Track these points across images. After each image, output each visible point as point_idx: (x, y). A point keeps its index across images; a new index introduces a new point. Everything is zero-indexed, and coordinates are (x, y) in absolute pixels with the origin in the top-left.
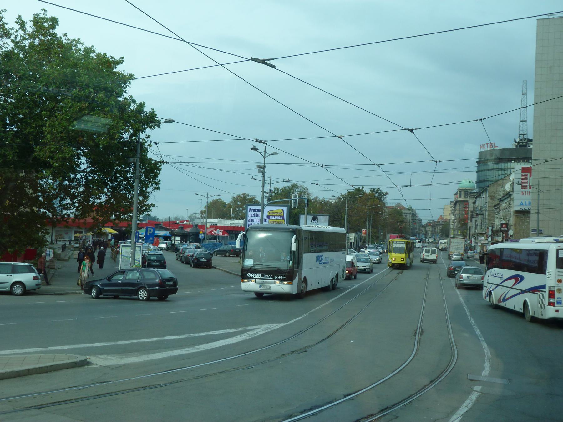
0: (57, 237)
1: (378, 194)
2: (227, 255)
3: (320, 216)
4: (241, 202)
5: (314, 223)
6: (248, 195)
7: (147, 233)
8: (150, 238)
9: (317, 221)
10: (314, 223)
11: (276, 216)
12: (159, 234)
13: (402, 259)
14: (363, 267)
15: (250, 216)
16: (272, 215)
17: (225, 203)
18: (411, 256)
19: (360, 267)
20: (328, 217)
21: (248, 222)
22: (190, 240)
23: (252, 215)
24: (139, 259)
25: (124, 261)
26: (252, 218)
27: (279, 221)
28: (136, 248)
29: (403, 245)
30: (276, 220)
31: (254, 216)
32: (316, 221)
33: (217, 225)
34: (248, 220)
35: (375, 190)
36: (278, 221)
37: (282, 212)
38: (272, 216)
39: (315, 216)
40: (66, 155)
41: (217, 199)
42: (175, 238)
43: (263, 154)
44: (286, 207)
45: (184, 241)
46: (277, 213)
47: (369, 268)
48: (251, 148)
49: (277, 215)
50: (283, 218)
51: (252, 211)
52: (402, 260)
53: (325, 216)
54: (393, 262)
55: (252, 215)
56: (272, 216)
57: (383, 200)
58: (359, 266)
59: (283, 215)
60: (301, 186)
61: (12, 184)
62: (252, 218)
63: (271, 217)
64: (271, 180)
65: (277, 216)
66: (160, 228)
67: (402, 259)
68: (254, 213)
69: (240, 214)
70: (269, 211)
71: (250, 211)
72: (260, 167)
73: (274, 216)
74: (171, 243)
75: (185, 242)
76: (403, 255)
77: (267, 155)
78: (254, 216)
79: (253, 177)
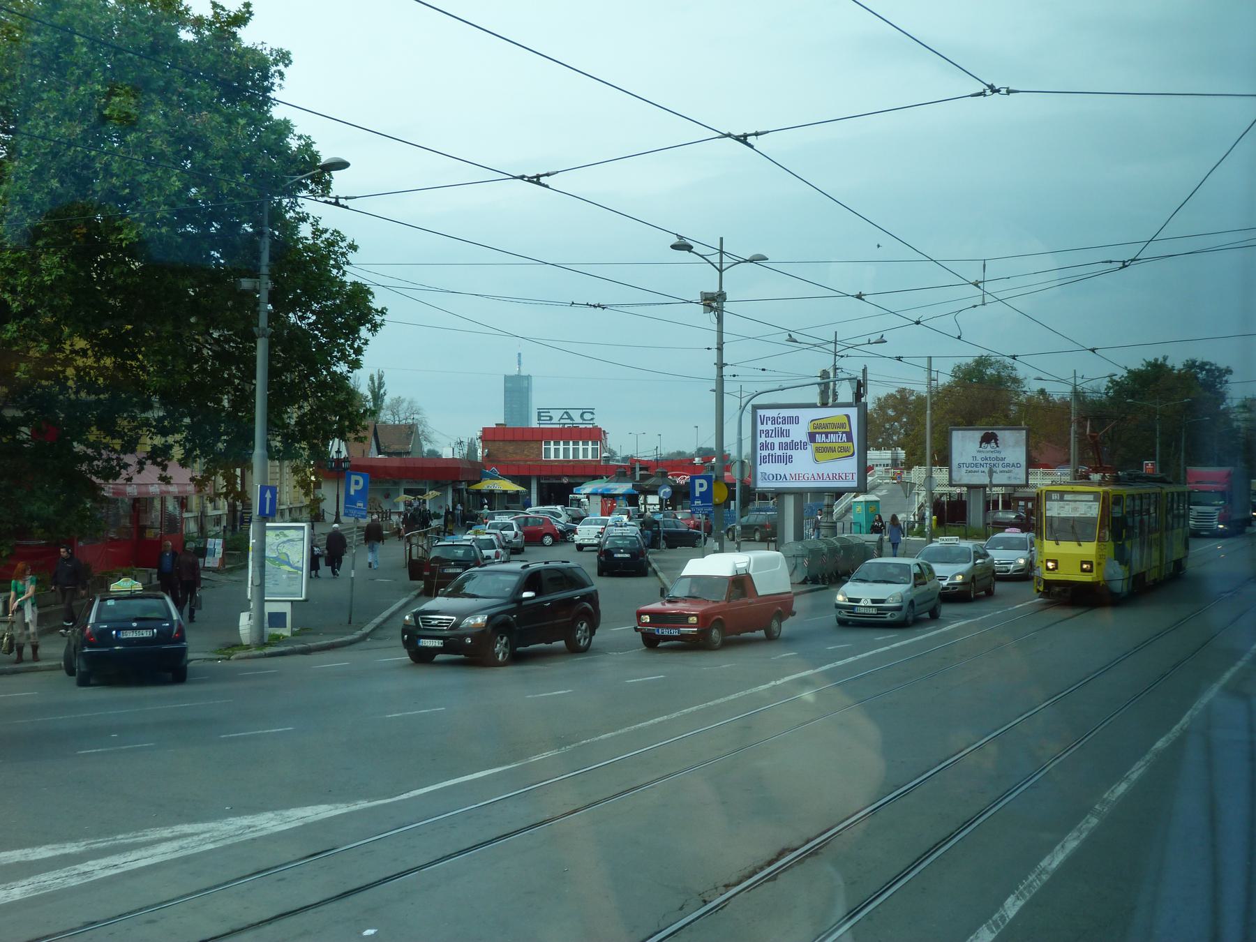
1: (1204, 372)
2: (757, 537)
3: (1002, 432)
4: (895, 408)
6: (912, 392)
7: (349, 491)
8: (358, 504)
9: (997, 444)
11: (831, 433)
12: (616, 489)
13: (1085, 566)
14: (874, 601)
15: (763, 435)
16: (821, 430)
20: (1025, 431)
21: (759, 452)
23: (767, 434)
26: (769, 440)
28: (269, 533)
29: (1090, 507)
30: (831, 445)
31: (773, 435)
32: (993, 444)
34: (759, 446)
35: (1197, 364)
37: (847, 422)
39: (990, 432)
40: (46, 278)
42: (645, 500)
43: (716, 259)
46: (834, 426)
47: (899, 609)
48: (672, 244)
49: (836, 430)
50: (850, 439)
51: (769, 422)
52: (1083, 570)
53: (1016, 431)
54: (1049, 576)
55: (768, 433)
56: (822, 433)
57: (1221, 387)
58: (858, 600)
59: (847, 429)
62: (769, 440)
63: (817, 435)
65: (834, 433)
66: (619, 476)
67: (1085, 566)
68: (773, 427)
69: (895, 438)
70: (812, 421)
71: (762, 424)
72: (709, 296)
73: (827, 434)
74: (639, 511)
75: (670, 508)
76: (1089, 549)
78: (773, 435)
79: (790, 335)
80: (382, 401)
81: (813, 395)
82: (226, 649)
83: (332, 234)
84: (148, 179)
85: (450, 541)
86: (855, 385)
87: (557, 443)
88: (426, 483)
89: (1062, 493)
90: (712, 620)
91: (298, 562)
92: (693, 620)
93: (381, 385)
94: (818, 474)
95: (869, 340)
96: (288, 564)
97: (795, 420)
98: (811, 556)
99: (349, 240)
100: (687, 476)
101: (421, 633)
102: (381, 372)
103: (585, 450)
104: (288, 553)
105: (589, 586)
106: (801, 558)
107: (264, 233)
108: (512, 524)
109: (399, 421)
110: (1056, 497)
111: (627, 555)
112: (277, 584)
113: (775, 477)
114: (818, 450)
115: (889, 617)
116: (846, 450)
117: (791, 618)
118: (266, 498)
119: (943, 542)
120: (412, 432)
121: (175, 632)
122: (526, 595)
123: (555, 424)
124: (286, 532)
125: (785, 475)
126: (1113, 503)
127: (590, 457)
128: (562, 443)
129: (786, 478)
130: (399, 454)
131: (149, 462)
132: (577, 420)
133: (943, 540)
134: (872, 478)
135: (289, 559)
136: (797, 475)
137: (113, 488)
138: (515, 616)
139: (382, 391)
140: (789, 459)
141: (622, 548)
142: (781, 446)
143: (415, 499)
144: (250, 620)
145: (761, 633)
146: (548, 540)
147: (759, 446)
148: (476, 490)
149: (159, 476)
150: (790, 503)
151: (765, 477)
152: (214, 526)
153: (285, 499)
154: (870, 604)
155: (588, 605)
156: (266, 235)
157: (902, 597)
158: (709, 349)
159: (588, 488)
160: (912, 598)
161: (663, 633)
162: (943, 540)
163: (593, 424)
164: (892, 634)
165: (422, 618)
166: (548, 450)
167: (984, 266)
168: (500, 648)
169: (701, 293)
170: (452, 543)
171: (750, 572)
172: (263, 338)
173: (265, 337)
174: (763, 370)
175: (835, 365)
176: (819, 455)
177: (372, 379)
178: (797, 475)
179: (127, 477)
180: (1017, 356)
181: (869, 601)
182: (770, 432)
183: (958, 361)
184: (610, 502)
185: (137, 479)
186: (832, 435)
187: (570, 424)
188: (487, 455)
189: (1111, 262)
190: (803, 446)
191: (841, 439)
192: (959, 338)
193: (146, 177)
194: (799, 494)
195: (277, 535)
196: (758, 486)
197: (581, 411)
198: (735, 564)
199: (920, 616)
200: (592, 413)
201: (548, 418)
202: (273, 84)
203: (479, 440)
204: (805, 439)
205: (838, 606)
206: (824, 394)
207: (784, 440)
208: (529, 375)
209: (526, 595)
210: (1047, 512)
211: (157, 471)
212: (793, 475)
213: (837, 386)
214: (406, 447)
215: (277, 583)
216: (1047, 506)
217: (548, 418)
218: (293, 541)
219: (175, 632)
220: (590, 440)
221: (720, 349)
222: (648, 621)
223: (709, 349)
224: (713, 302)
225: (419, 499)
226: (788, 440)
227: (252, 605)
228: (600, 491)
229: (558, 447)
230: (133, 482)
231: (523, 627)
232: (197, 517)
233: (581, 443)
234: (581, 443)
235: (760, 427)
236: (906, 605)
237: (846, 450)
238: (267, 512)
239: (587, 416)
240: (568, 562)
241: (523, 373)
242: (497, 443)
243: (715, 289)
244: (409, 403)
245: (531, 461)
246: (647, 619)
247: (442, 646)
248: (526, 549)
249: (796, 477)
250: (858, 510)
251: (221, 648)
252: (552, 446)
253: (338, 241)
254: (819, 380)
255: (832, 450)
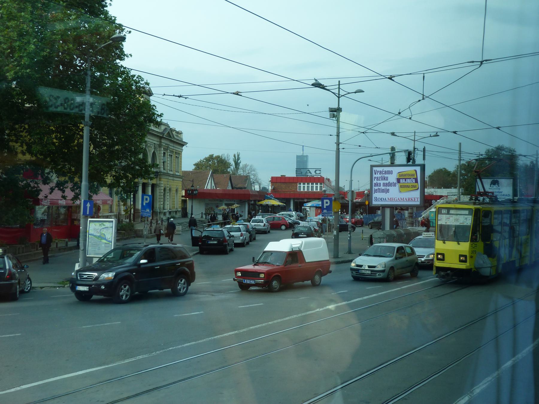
0: (207, 210)
4: (465, 170)
5: (494, 188)
8: (147, 210)
10: (494, 188)
14: (369, 267)
15: (376, 179)
17: (450, 172)
18: (23, 282)
19: (363, 268)
21: (374, 187)
22: (361, 211)
23: (378, 179)
24: (111, 238)
25: (92, 242)
26: (379, 182)
27: (412, 184)
29: (466, 219)
31: (380, 179)
32: (497, 186)
33: (433, 194)
34: (374, 185)
36: (410, 184)
38: (403, 179)
39: (495, 179)
41: (442, 168)
43: (336, 91)
44: (420, 167)
45: (345, 212)
46: (409, 175)
47: (383, 271)
49: (409, 177)
50: (416, 181)
51: (379, 173)
56: (403, 179)
58: (361, 266)
59: (415, 177)
60: (506, 148)
61: (37, 151)
62: (379, 182)
64: (415, 135)
68: (380, 176)
70: (399, 172)
71: (375, 174)
77: (340, 96)
78: (380, 179)
80: (239, 165)
81: (387, 159)
82: (66, 282)
83: (137, 78)
84: (18, 44)
85: (212, 228)
86: (407, 154)
87: (304, 184)
88: (235, 201)
89: (449, 209)
90: (272, 276)
91: (110, 238)
92: (262, 276)
93: (238, 159)
94: (401, 198)
95: (430, 135)
96: (105, 239)
97: (391, 172)
98: (388, 238)
99: (145, 81)
100: (360, 199)
101: (78, 282)
102: (238, 153)
103: (317, 187)
104: (106, 234)
105: (188, 258)
106: (382, 239)
107: (88, 74)
108: (263, 220)
109: (246, 174)
110: (444, 212)
111: (215, 242)
112: (100, 249)
113: (381, 199)
114: (401, 187)
115: (378, 276)
116: (415, 187)
117: (329, 274)
118: (87, 207)
119: (425, 235)
120: (247, 179)
121: (6, 275)
122: (142, 261)
123: (303, 175)
124: (105, 223)
125: (385, 198)
126: (483, 216)
127: (319, 190)
128: (306, 184)
129: (406, 200)
130: (241, 188)
131: (57, 189)
132: (313, 173)
133: (425, 234)
134: (443, 201)
135: (105, 237)
136: (391, 198)
137: (50, 201)
138: (134, 274)
139: (239, 161)
140: (387, 191)
141: (303, 232)
142: (384, 185)
143: (227, 208)
144: (79, 267)
145: (309, 282)
146: (283, 227)
147: (374, 185)
148: (260, 204)
149: (61, 195)
150: (388, 212)
151: (376, 199)
152: (125, 219)
153: (166, 207)
154: (367, 268)
155: (187, 269)
156: (89, 75)
157: (385, 265)
158: (331, 135)
159: (309, 204)
160: (393, 265)
161: (247, 282)
162: (425, 234)
163: (321, 175)
164: (379, 286)
165: (80, 274)
166: (300, 187)
167: (424, 77)
168: (124, 292)
169: (329, 108)
170: (213, 229)
171: (302, 250)
172: (87, 127)
173: (88, 126)
174: (360, 146)
175: (414, 147)
176: (402, 189)
177: (235, 156)
178: (391, 198)
179: (45, 196)
180: (457, 132)
181: (367, 266)
182: (379, 178)
183: (488, 148)
184: (320, 210)
185: (50, 197)
186: (408, 179)
187: (310, 175)
188: (273, 189)
189: (473, 62)
190: (394, 185)
191: (413, 182)
192: (410, 118)
193: (18, 44)
194: (393, 208)
195: (100, 225)
196: (373, 204)
197: (315, 170)
198: (292, 245)
199: (403, 275)
200: (320, 171)
201: (300, 173)
202: (106, 3)
203: (270, 182)
204: (395, 181)
205: (352, 269)
206: (409, 160)
207: (385, 182)
208: (307, 155)
209: (142, 261)
210: (438, 221)
211: (60, 193)
212: (402, 198)
213: (415, 157)
214: (245, 185)
215: (99, 248)
216: (439, 217)
217: (300, 173)
218: (107, 228)
219: (6, 275)
220: (319, 182)
221: (338, 136)
222: (240, 275)
223: (331, 135)
224: (335, 112)
225: (229, 208)
226: (387, 182)
227: (80, 260)
228: (315, 205)
229: (317, 185)
230: (48, 198)
231: (140, 280)
232: (116, 215)
233: (315, 184)
234: (315, 184)
235: (374, 176)
236: (387, 269)
237: (415, 187)
238: (88, 213)
239: (318, 172)
240: (176, 244)
241: (305, 154)
242: (278, 184)
243: (335, 106)
244: (251, 167)
245: (293, 192)
246: (239, 274)
247: (88, 290)
248: (271, 231)
249: (391, 199)
250: (432, 215)
251: (64, 281)
252: (302, 185)
253: (140, 81)
254: (390, 152)
255: (408, 187)
